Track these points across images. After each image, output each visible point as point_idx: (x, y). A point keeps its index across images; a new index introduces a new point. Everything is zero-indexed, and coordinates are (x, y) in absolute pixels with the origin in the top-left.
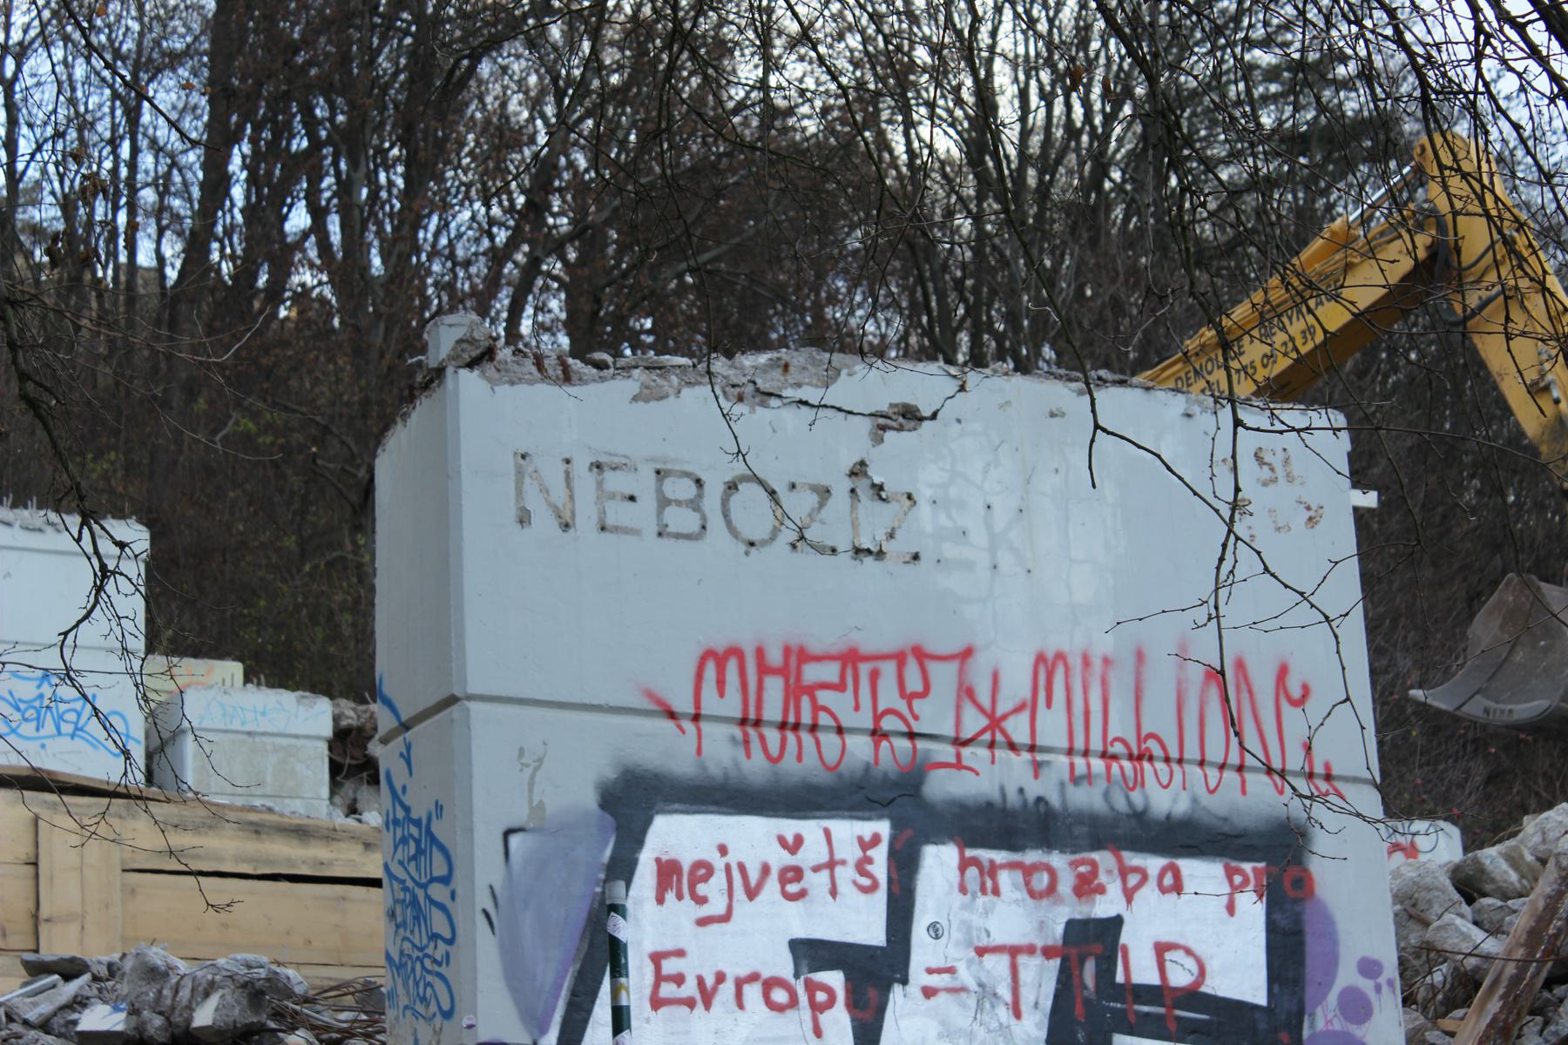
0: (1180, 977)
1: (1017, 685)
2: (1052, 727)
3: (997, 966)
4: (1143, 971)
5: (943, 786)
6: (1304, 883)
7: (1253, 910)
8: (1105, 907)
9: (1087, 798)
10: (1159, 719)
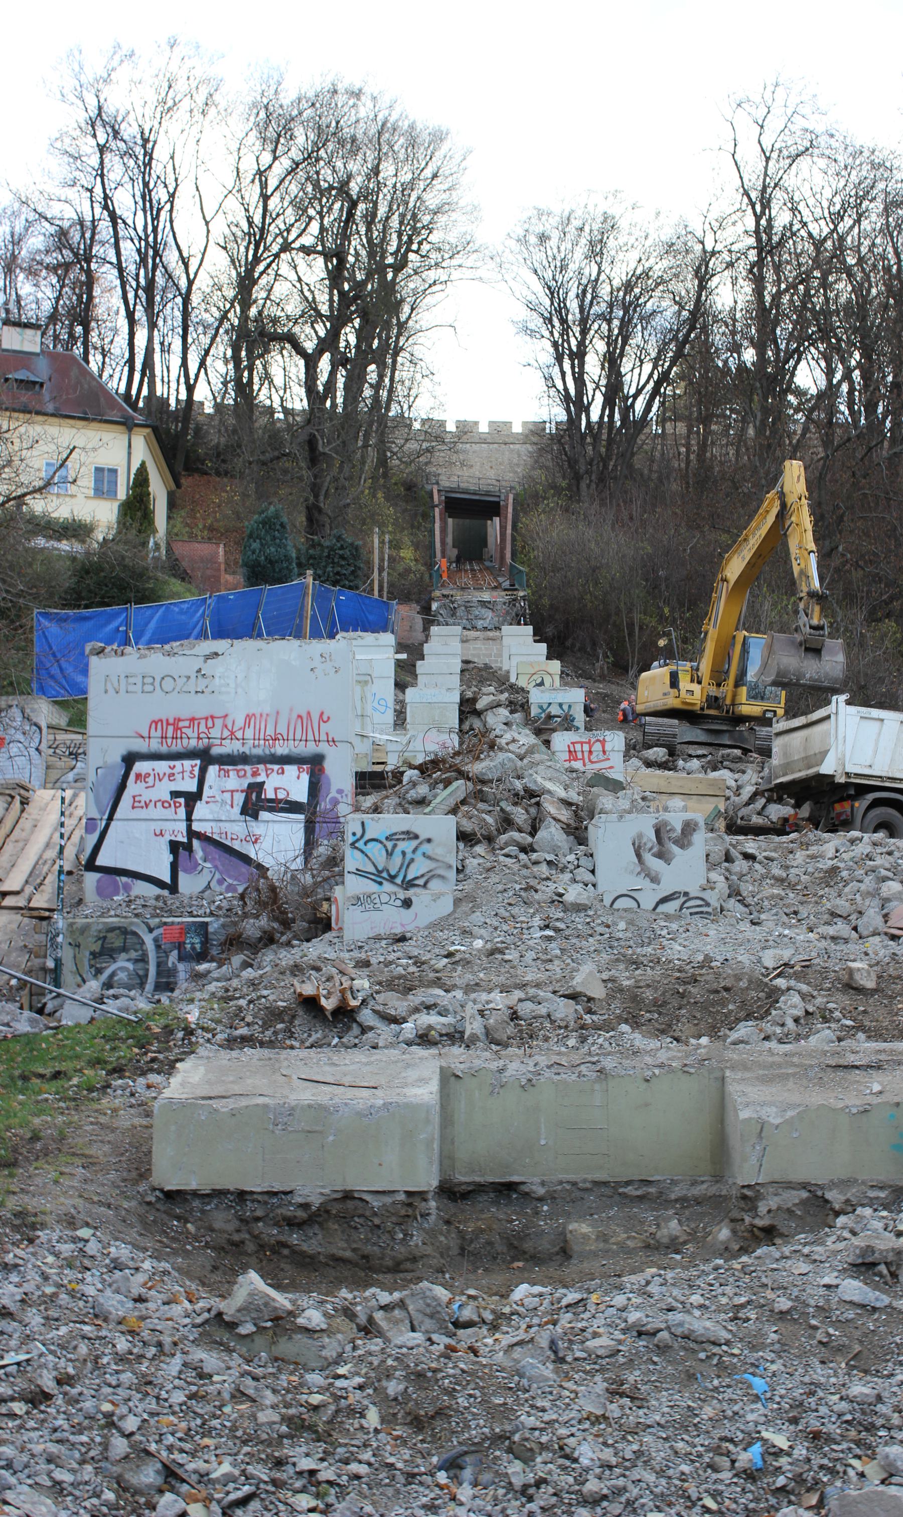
0: (281, 795)
1: (240, 723)
2: (249, 733)
3: (227, 796)
4: (270, 795)
5: (215, 751)
6: (322, 770)
7: (305, 778)
8: (259, 779)
9: (258, 751)
10: (282, 729)
